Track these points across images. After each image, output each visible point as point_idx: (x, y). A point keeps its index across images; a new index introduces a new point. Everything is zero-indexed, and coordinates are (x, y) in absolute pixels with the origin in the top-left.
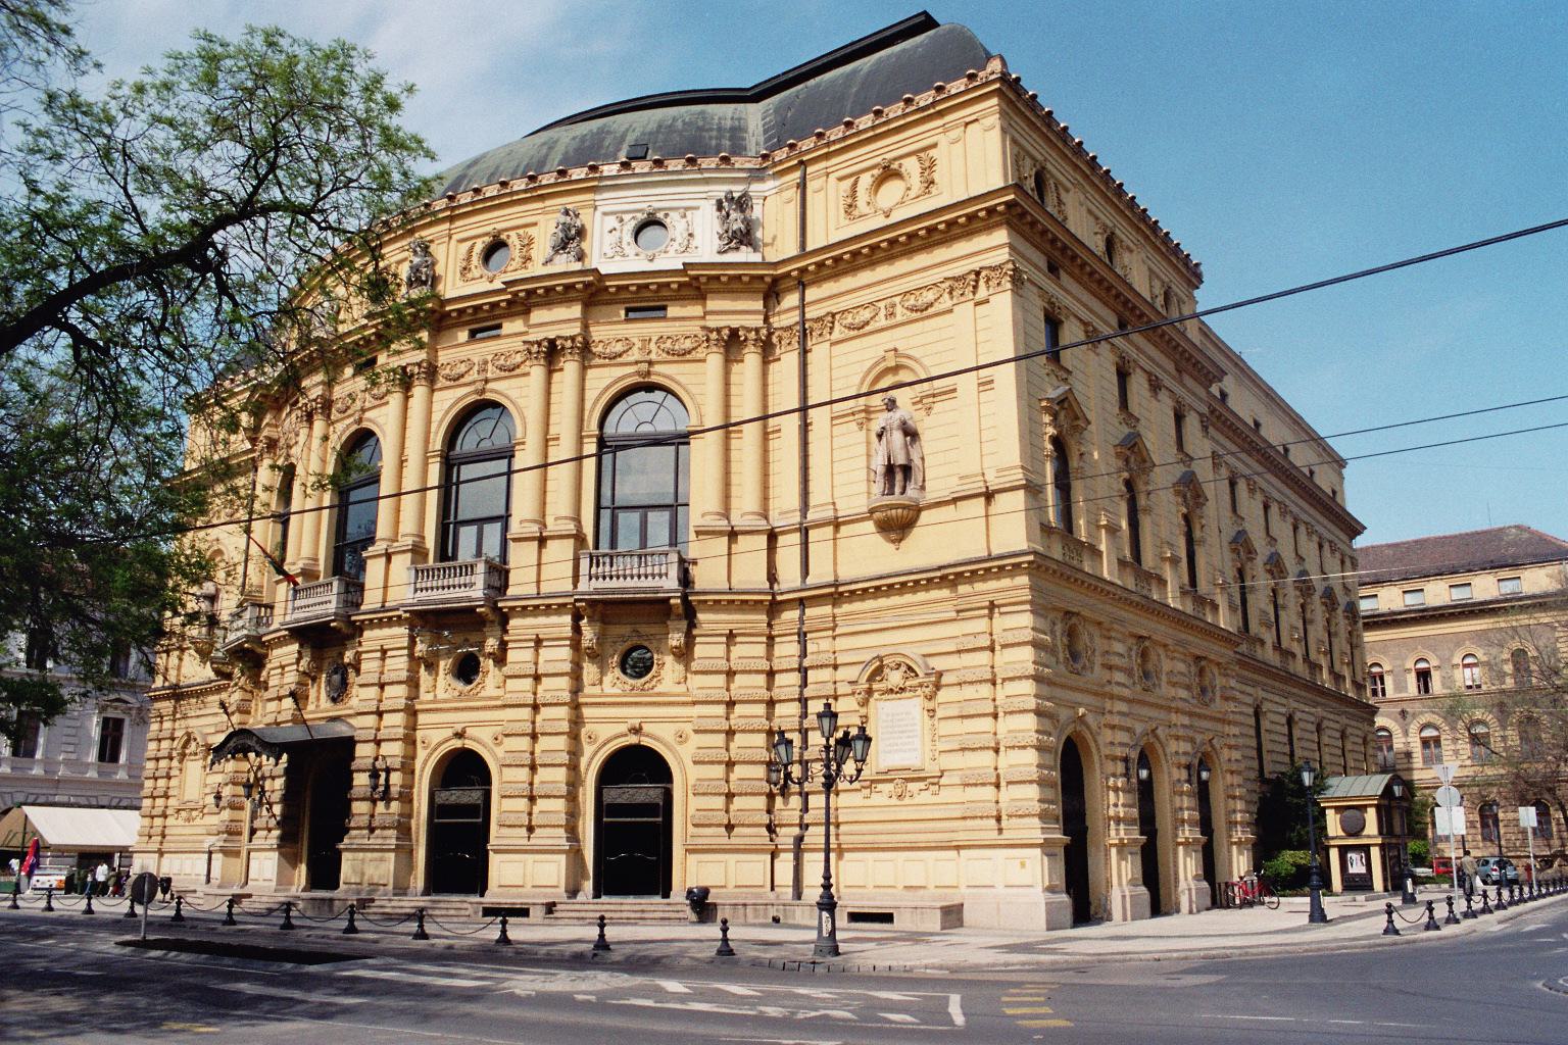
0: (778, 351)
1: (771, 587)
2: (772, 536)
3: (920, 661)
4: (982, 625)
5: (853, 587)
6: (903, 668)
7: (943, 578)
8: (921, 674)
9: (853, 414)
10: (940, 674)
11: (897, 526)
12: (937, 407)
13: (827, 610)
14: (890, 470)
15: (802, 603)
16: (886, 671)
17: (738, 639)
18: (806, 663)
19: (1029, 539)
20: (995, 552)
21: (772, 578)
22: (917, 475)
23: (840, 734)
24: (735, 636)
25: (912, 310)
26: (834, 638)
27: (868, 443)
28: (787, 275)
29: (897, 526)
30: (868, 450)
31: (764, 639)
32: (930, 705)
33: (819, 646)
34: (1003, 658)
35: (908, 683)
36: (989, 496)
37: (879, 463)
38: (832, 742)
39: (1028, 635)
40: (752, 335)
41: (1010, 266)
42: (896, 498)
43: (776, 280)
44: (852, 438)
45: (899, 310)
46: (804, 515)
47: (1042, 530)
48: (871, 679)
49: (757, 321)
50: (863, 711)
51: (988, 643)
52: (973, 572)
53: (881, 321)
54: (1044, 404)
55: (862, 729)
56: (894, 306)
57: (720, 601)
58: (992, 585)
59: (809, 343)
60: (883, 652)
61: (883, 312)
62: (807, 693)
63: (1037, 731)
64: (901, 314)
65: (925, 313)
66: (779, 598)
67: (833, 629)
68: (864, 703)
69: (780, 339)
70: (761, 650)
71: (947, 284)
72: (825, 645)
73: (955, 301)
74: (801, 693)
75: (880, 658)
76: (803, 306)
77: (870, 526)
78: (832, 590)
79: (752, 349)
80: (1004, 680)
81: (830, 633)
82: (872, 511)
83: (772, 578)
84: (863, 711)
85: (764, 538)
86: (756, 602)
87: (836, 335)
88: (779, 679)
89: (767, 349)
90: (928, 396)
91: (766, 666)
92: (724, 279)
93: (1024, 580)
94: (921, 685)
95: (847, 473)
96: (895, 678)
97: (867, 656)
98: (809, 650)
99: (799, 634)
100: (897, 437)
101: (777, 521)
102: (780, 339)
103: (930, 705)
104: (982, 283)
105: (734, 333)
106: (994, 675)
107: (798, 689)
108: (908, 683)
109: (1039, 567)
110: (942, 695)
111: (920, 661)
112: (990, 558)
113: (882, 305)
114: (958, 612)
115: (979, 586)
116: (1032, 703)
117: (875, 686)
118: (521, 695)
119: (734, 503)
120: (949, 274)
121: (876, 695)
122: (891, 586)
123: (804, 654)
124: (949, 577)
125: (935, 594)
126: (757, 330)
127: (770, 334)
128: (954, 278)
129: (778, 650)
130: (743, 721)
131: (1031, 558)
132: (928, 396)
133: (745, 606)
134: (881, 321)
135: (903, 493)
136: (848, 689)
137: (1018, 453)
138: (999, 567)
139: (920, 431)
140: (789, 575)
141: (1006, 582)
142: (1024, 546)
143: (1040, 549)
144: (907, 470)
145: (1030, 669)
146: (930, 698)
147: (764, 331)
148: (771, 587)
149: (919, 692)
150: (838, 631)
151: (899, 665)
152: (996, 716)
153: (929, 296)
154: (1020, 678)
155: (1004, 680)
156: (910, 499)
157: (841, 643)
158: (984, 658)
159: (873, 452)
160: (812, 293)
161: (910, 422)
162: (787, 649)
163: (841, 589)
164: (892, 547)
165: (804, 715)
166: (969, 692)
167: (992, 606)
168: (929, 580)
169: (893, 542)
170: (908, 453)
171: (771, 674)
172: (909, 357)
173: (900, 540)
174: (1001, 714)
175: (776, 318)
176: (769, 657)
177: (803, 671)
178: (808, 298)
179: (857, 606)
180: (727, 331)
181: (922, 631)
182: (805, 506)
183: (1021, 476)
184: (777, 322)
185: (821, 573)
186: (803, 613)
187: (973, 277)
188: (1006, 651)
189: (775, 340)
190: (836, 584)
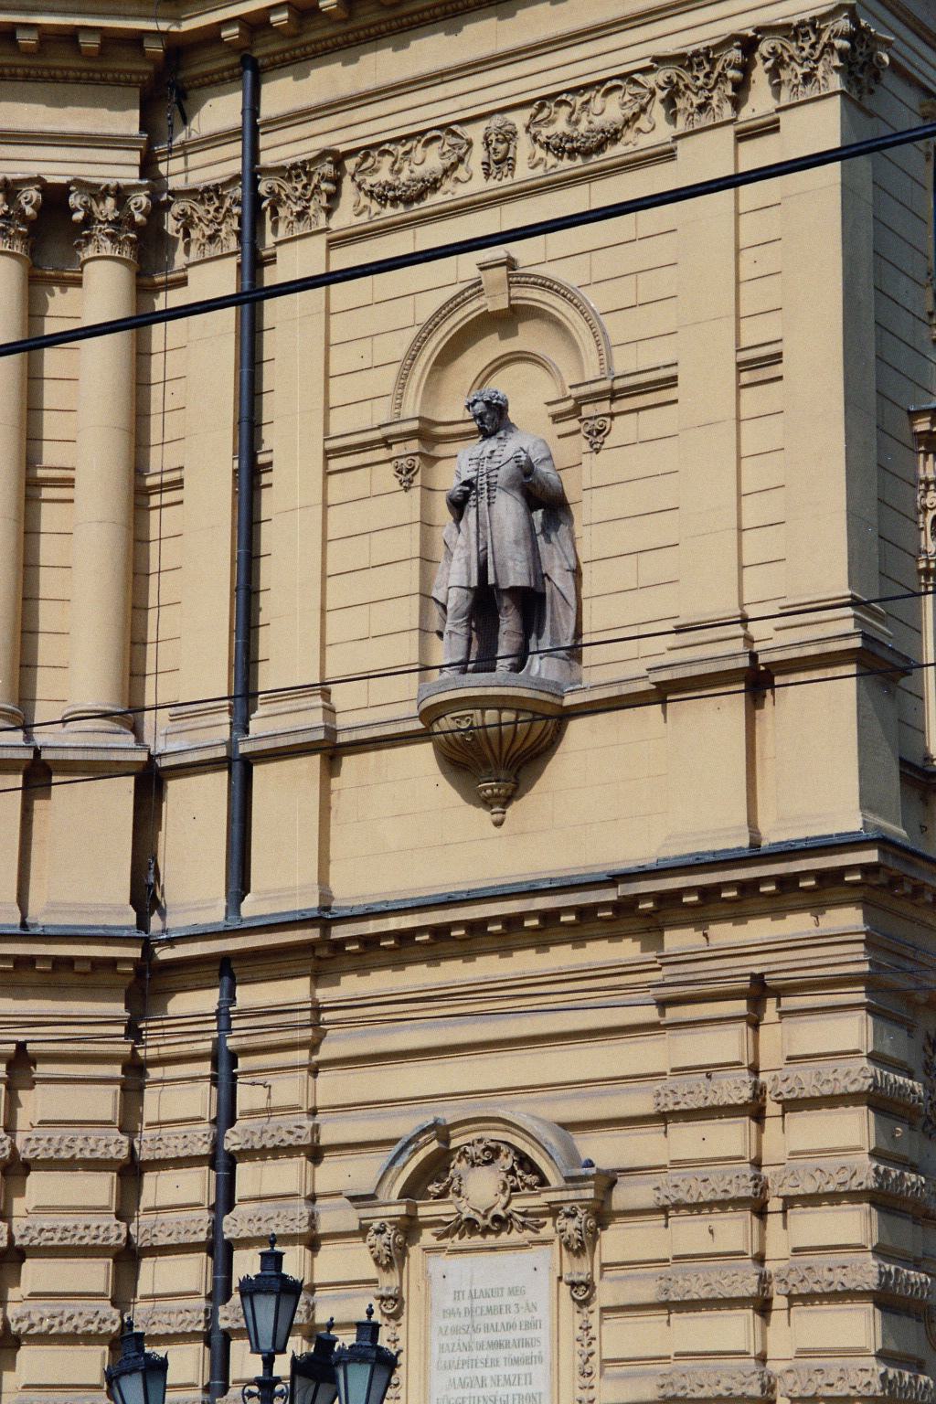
0: (180, 259)
1: (142, 923)
2: (150, 783)
3: (550, 1138)
4: (726, 1044)
5: (372, 927)
6: (507, 1161)
7: (625, 907)
8: (554, 1179)
9: (386, 442)
10: (608, 1181)
11: (497, 759)
12: (622, 429)
13: (296, 990)
14: (484, 602)
15: (227, 971)
16: (459, 1167)
17: (42, 1070)
18: (232, 1141)
19: (867, 803)
20: (773, 835)
21: (145, 895)
22: (559, 624)
23: (298, 1345)
24: (34, 1060)
25: (560, 148)
26: (314, 1071)
27: (427, 524)
28: (210, 36)
29: (497, 759)
30: (426, 543)
31: (116, 1071)
32: (579, 1269)
33: (270, 1092)
34: (790, 1137)
35: (517, 1204)
36: (758, 681)
37: (455, 578)
38: (282, 1367)
39: (859, 1075)
40: (108, 207)
41: (844, 24)
42: (498, 682)
43: (179, 49)
44: (382, 508)
45: (524, 149)
46: (241, 725)
47: (904, 777)
48: (413, 1191)
49: (121, 169)
50: (389, 1282)
51: (746, 1093)
52: (709, 893)
53: (474, 182)
54: (923, 425)
55: (369, 1329)
56: (508, 136)
57: (31, 960)
58: (761, 929)
59: (270, 239)
60: (449, 1114)
61: (478, 155)
62: (233, 1227)
63: (882, 1356)
64: (528, 162)
65: (597, 161)
66: (164, 954)
67: (314, 1047)
68: (393, 1260)
69: (187, 223)
70: (104, 1102)
71: (660, 76)
72: (288, 1090)
73: (682, 125)
74: (215, 1227)
75: (441, 1131)
76: (252, 129)
77: (424, 754)
78: (312, 934)
79: (108, 248)
80: (789, 1202)
81: (302, 1056)
82: (431, 714)
83: (145, 895)
84: (389, 1282)
85: (125, 787)
86: (97, 963)
87: (344, 218)
88: (156, 1188)
89: (149, 252)
90: (596, 397)
91: (113, 1145)
92: (27, 39)
93: (848, 918)
94: (553, 1210)
95: (361, 603)
96: (481, 1188)
97: (403, 1125)
98: (243, 1103)
99: (214, 1057)
100: (507, 511)
101: (166, 738)
102: (187, 223)
103: (579, 1269)
104: (759, 75)
105: (55, 196)
106: (761, 1186)
107: (205, 1216)
108: (517, 1204)
109: (895, 882)
110: (614, 1242)
111: (550, 1138)
112: (755, 855)
113: (475, 132)
114: (663, 1004)
115: (725, 934)
116: (867, 1272)
117: (425, 1211)
118: (70, 1307)
119: (45, 683)
120: (668, 47)
121: (427, 1238)
122: (476, 927)
123: (227, 1115)
124: (635, 905)
125: (600, 952)
126: (121, 194)
127: (158, 210)
128: (679, 59)
129: (155, 1104)
130: (46, 1308)
131: (871, 856)
132: (596, 397)
133: (64, 976)
134: (474, 182)
135: (520, 663)
136: (347, 1218)
137: (42, 510)
138: (781, 880)
139: (571, 496)
140: (195, 890)
141: (798, 924)
142: (851, 822)
143: (898, 831)
144: (531, 603)
145: (864, 1172)
146: (581, 1247)
147: (142, 199)
148: (142, 923)
149: (547, 1231)
150: (326, 1051)
151: (496, 1152)
152: (763, 1307)
153: (611, 110)
154: (834, 1198)
155: (789, 1202)
156: (540, 685)
157: (332, 1087)
158: (730, 1137)
159: (439, 553)
160: (279, 95)
161: (544, 469)
162: (179, 1101)
163: (338, 932)
164: (483, 816)
165: (220, 1292)
166: (690, 1234)
167: (759, 991)
168: (584, 912)
169: (486, 803)
170: (535, 558)
171: (131, 1172)
172: (547, 285)
173: (507, 800)
174: (779, 1302)
175: (177, 164)
176: (129, 1121)
177: (223, 1163)
178: (268, 109)
179: (382, 981)
180: (33, 194)
181: (565, 1059)
182: (245, 696)
183: (849, 626)
184: (177, 173)
185: (283, 884)
186: (231, 997)
187: (735, 55)
188: (798, 1120)
189: (171, 225)
190: (324, 918)
